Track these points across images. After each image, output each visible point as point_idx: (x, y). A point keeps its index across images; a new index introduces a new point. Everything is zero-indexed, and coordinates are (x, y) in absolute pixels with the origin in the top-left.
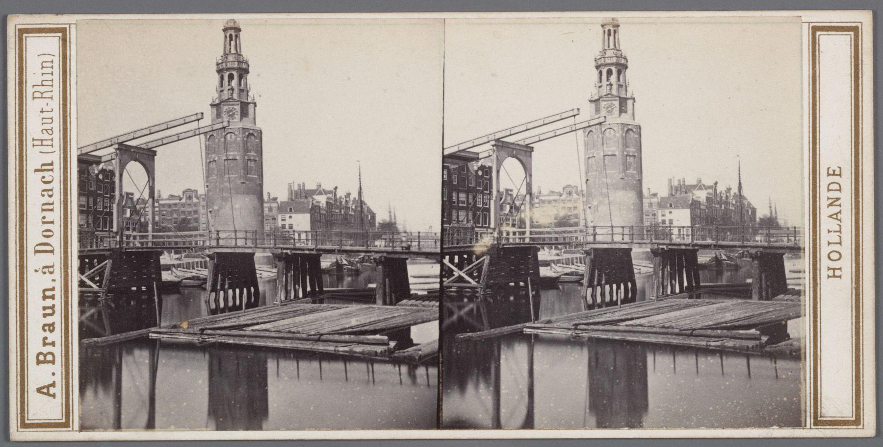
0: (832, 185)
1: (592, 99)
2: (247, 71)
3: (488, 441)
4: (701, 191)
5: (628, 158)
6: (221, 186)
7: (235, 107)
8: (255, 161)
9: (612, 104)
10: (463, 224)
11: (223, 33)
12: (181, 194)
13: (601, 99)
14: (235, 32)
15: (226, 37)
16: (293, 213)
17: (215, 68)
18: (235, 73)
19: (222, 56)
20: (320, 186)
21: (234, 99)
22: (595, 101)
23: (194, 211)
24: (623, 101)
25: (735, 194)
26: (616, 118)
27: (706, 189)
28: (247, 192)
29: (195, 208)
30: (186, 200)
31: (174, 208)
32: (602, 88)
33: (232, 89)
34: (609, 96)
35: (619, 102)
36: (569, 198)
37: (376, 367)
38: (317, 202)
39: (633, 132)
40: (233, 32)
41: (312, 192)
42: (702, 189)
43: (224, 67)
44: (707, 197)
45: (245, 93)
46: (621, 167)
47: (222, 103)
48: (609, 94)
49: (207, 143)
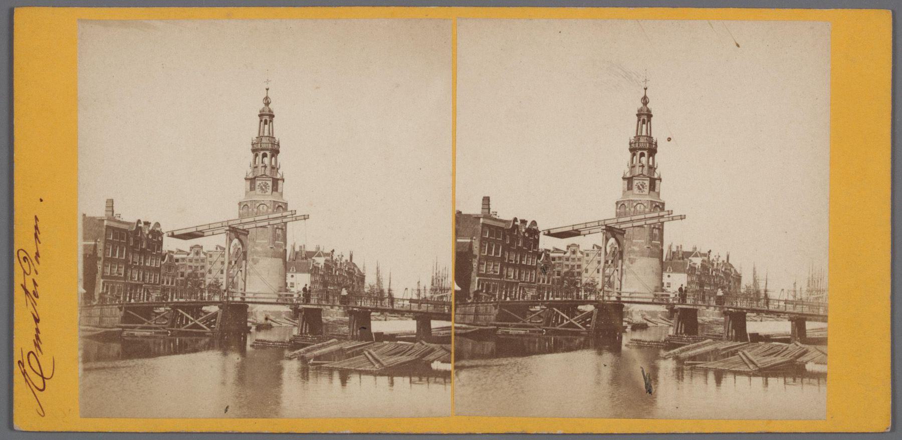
0: (23, 252)
1: (248, 177)
2: (277, 152)
3: (787, 435)
4: (320, 258)
5: (654, 230)
6: (629, 249)
7: (268, 182)
8: (282, 229)
9: (643, 182)
10: (510, 279)
11: (259, 118)
12: (188, 250)
13: (257, 179)
14: (269, 118)
15: (261, 121)
16: (672, 273)
17: (250, 147)
18: (268, 153)
19: (257, 138)
20: (696, 248)
21: (267, 176)
22: (251, 179)
23: (578, 265)
24: (275, 182)
25: (347, 261)
26: (269, 195)
27: (701, 256)
28: (652, 255)
29: (202, 264)
30: (194, 255)
31: (181, 263)
32: (635, 168)
33: (265, 167)
34: (264, 176)
35: (650, 182)
36: (196, 257)
37: (377, 377)
38: (694, 264)
39: (283, 208)
40: (267, 118)
41: (687, 255)
42: (698, 257)
43: (259, 147)
44: (701, 264)
45: (275, 170)
46: (648, 238)
47: (634, 178)
48: (641, 174)
49: (241, 211)
